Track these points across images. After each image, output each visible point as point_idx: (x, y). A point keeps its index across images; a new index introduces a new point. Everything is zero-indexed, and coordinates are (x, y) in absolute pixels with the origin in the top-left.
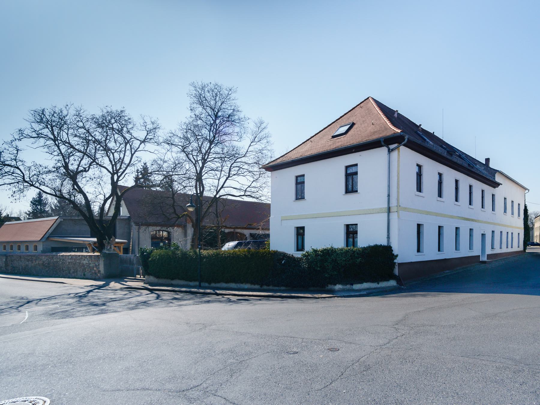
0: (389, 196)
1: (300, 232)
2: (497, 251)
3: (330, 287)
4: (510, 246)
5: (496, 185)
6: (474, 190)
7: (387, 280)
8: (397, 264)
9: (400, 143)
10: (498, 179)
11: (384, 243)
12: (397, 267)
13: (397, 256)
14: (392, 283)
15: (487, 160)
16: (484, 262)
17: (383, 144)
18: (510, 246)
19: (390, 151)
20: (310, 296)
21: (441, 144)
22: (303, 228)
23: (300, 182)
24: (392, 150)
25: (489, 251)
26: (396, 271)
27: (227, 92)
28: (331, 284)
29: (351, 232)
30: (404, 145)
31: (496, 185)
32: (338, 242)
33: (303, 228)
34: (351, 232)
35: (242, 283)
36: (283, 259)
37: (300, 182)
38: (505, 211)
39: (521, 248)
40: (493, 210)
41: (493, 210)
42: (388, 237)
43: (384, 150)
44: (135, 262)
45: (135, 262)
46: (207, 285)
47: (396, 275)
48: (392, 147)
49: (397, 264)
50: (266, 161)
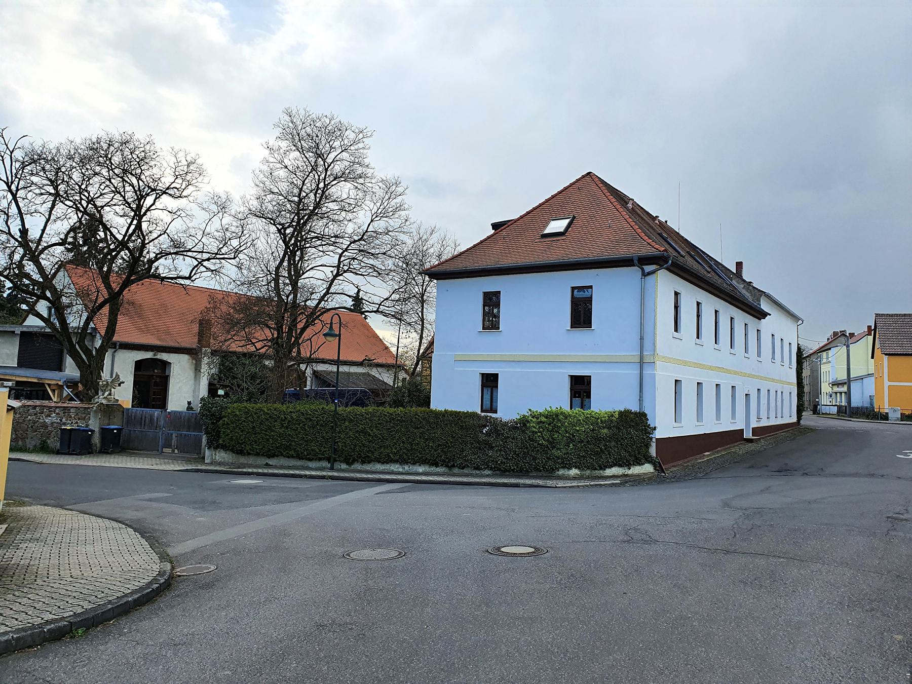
0: (642, 339)
1: (490, 381)
2: (764, 423)
3: (561, 472)
4: (779, 415)
5: (761, 315)
6: (704, 307)
7: (640, 464)
8: (654, 440)
9: (661, 267)
10: (765, 306)
11: (635, 408)
12: (654, 445)
13: (655, 428)
14: (648, 468)
15: (739, 265)
16: (749, 441)
17: (636, 262)
18: (779, 415)
19: (645, 275)
20: (540, 482)
21: (660, 231)
22: (496, 376)
23: (491, 301)
24: (649, 274)
25: (754, 424)
26: (653, 451)
27: (352, 136)
28: (563, 468)
29: (580, 387)
30: (667, 269)
31: (761, 315)
32: (559, 400)
33: (496, 376)
34: (580, 387)
35: (414, 464)
36: (485, 426)
37: (491, 301)
38: (773, 358)
39: (794, 420)
40: (759, 355)
41: (759, 355)
42: (641, 400)
43: (633, 273)
44: (162, 423)
45: (162, 423)
46: (344, 466)
47: (651, 457)
48: (648, 268)
49: (654, 440)
50: (432, 262)
